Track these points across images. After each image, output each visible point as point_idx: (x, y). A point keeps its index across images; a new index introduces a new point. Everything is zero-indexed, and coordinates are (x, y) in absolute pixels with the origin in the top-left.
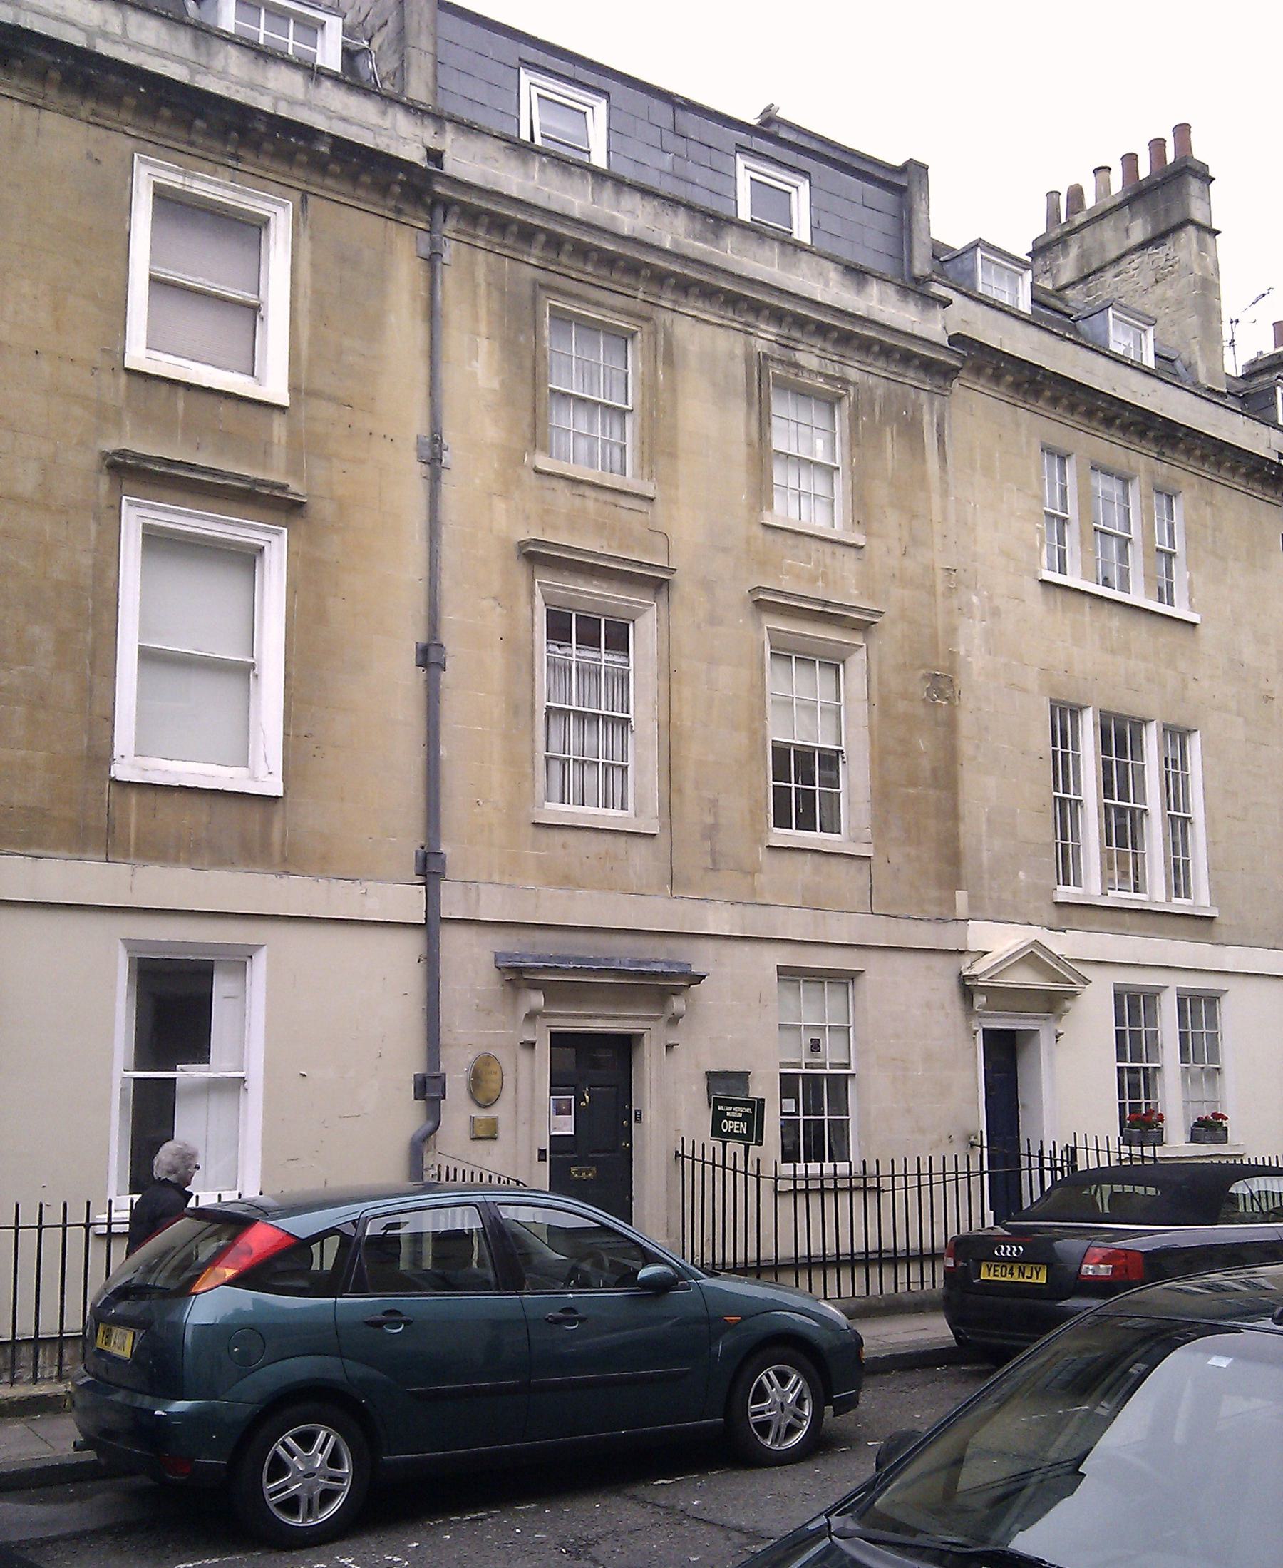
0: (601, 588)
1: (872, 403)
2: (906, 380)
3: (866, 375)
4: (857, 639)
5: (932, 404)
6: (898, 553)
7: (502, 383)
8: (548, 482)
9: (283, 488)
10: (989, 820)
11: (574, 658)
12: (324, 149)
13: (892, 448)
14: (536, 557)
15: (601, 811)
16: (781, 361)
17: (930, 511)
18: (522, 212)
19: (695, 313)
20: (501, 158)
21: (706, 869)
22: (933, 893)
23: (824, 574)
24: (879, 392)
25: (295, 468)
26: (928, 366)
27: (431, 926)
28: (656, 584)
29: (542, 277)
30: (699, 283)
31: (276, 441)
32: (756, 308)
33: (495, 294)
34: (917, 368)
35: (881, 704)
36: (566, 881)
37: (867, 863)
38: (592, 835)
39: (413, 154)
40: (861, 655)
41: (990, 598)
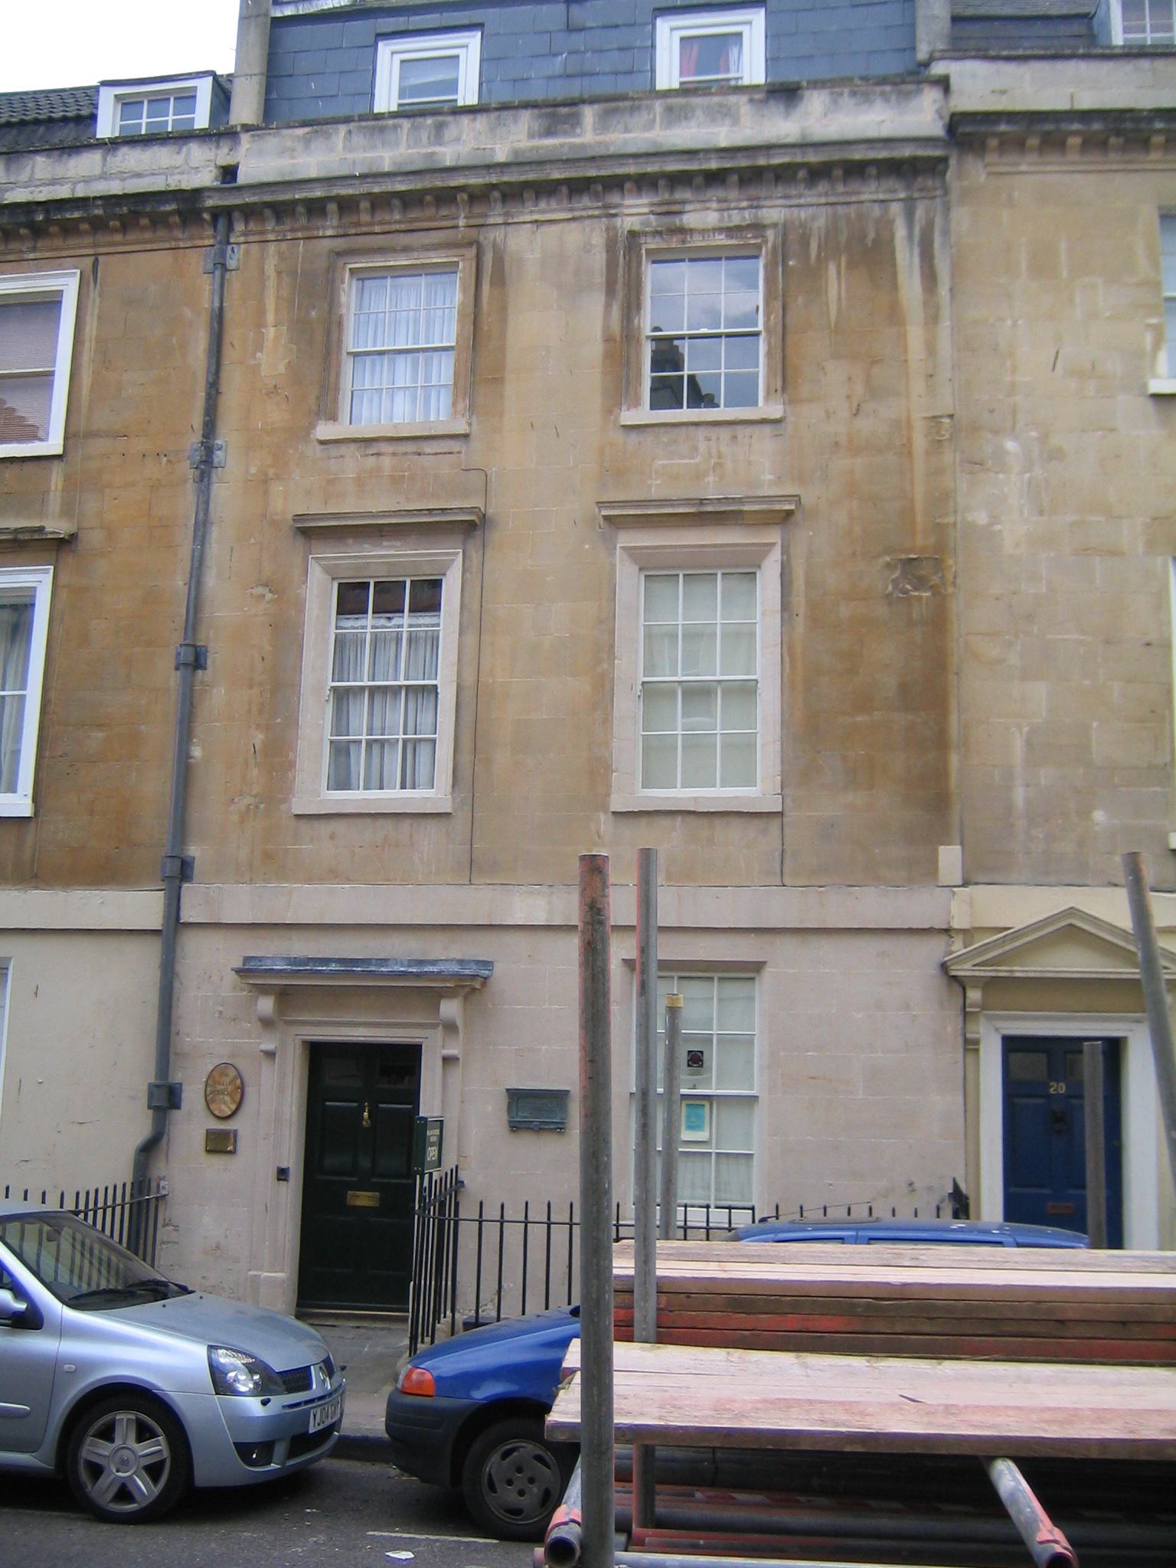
1: (805, 241)
3: (795, 210)
4: (774, 536)
7: (289, 365)
8: (334, 451)
9: (41, 529)
10: (1029, 745)
11: (369, 630)
12: (99, 212)
13: (835, 284)
14: (312, 532)
15: (375, 794)
17: (905, 351)
24: (821, 223)
25: (68, 510)
27: (173, 929)
28: (471, 528)
29: (341, 244)
32: (616, 184)
33: (286, 279)
34: (878, 177)
38: (368, 821)
39: (206, 178)
41: (1044, 438)
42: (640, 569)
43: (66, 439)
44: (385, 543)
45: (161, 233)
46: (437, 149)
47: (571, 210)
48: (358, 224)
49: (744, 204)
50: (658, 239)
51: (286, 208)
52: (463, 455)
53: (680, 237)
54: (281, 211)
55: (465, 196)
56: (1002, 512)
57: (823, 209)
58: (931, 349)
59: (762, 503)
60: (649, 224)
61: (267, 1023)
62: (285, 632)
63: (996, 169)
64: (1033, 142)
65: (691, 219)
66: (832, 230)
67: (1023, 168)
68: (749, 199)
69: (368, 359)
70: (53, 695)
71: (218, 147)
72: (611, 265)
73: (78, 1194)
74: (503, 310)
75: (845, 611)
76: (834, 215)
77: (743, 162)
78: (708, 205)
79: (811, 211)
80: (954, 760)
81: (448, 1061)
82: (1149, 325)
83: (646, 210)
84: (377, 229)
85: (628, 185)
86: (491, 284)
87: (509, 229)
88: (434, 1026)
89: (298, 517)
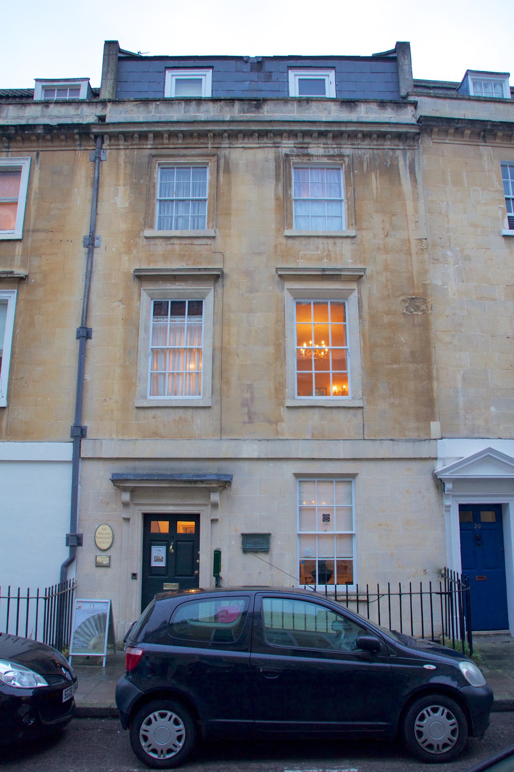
0: (180, 285)
1: (361, 163)
2: (385, 147)
3: (357, 150)
4: (354, 286)
5: (405, 156)
6: (382, 236)
7: (130, 204)
8: (152, 242)
9: (12, 272)
10: (464, 379)
13: (375, 183)
14: (142, 277)
15: (173, 397)
16: (298, 156)
18: (137, 127)
19: (243, 145)
20: (135, 109)
21: (244, 423)
22: (413, 424)
23: (328, 255)
24: (367, 156)
26: (399, 136)
28: (216, 277)
29: (154, 152)
30: (240, 131)
31: (17, 254)
32: (279, 134)
33: (129, 166)
34: (391, 140)
35: (372, 321)
36: (155, 435)
37: (360, 411)
38: (172, 410)
39: (92, 119)
40: (355, 294)
41: (462, 251)
42: (294, 299)
43: (23, 232)
44: (177, 284)
45: (70, 143)
46: (198, 114)
47: (259, 144)
48: (163, 144)
49: (335, 146)
50: (298, 158)
51: (131, 135)
52: (212, 246)
53: (307, 158)
54: (127, 136)
55: (212, 135)
56: (446, 280)
57: (368, 151)
58: (416, 211)
59: (350, 271)
60: (294, 152)
61: (126, 505)
62: (131, 323)
63: (436, 141)
64: (452, 131)
65: (311, 151)
66: (372, 159)
67: (447, 141)
68: (336, 144)
69: (166, 203)
70: (17, 350)
71: (96, 107)
72: (277, 168)
73: (46, 589)
74: (229, 184)
75: (386, 319)
76: (373, 153)
77: (336, 128)
78: (319, 145)
79: (363, 151)
80: (435, 384)
81: (214, 521)
82: (500, 208)
83: (292, 146)
84: (171, 146)
85: (285, 135)
86: (224, 173)
87: (231, 150)
88: (206, 505)
89: (137, 270)
